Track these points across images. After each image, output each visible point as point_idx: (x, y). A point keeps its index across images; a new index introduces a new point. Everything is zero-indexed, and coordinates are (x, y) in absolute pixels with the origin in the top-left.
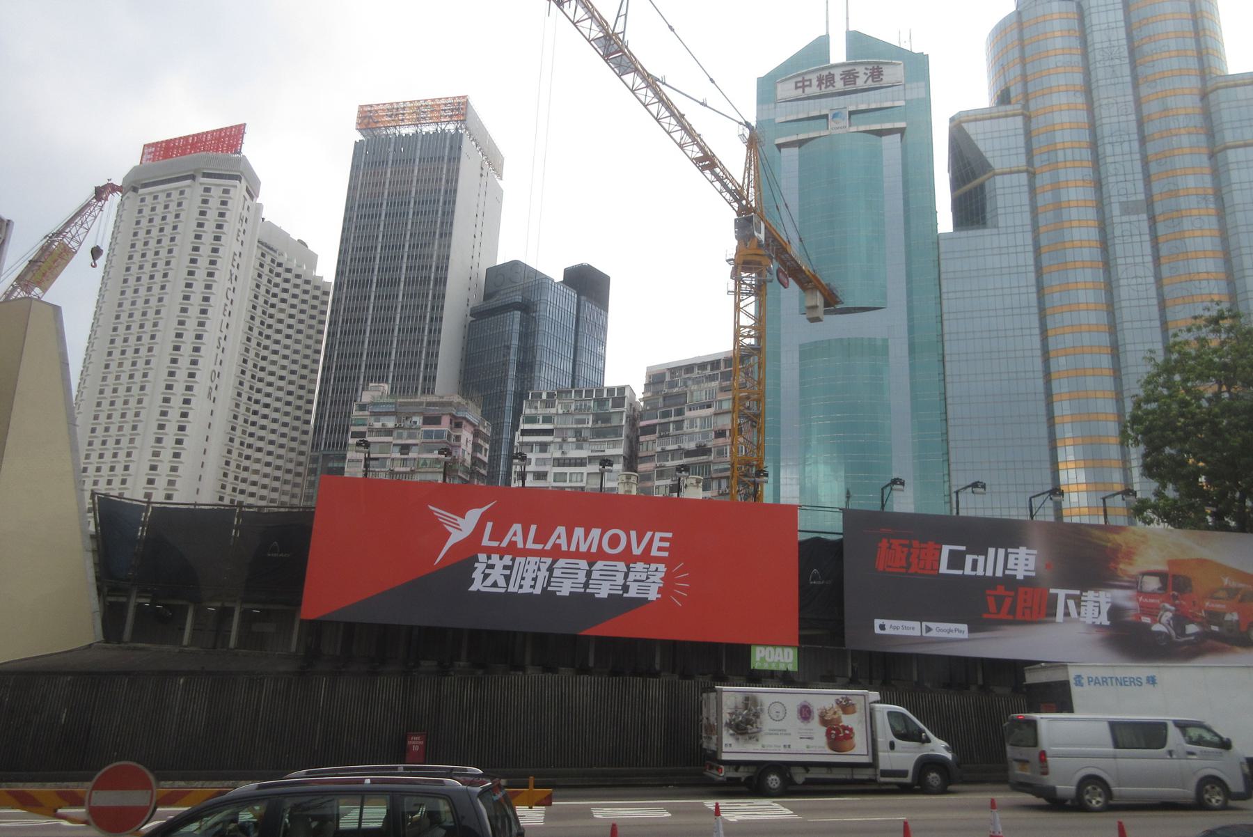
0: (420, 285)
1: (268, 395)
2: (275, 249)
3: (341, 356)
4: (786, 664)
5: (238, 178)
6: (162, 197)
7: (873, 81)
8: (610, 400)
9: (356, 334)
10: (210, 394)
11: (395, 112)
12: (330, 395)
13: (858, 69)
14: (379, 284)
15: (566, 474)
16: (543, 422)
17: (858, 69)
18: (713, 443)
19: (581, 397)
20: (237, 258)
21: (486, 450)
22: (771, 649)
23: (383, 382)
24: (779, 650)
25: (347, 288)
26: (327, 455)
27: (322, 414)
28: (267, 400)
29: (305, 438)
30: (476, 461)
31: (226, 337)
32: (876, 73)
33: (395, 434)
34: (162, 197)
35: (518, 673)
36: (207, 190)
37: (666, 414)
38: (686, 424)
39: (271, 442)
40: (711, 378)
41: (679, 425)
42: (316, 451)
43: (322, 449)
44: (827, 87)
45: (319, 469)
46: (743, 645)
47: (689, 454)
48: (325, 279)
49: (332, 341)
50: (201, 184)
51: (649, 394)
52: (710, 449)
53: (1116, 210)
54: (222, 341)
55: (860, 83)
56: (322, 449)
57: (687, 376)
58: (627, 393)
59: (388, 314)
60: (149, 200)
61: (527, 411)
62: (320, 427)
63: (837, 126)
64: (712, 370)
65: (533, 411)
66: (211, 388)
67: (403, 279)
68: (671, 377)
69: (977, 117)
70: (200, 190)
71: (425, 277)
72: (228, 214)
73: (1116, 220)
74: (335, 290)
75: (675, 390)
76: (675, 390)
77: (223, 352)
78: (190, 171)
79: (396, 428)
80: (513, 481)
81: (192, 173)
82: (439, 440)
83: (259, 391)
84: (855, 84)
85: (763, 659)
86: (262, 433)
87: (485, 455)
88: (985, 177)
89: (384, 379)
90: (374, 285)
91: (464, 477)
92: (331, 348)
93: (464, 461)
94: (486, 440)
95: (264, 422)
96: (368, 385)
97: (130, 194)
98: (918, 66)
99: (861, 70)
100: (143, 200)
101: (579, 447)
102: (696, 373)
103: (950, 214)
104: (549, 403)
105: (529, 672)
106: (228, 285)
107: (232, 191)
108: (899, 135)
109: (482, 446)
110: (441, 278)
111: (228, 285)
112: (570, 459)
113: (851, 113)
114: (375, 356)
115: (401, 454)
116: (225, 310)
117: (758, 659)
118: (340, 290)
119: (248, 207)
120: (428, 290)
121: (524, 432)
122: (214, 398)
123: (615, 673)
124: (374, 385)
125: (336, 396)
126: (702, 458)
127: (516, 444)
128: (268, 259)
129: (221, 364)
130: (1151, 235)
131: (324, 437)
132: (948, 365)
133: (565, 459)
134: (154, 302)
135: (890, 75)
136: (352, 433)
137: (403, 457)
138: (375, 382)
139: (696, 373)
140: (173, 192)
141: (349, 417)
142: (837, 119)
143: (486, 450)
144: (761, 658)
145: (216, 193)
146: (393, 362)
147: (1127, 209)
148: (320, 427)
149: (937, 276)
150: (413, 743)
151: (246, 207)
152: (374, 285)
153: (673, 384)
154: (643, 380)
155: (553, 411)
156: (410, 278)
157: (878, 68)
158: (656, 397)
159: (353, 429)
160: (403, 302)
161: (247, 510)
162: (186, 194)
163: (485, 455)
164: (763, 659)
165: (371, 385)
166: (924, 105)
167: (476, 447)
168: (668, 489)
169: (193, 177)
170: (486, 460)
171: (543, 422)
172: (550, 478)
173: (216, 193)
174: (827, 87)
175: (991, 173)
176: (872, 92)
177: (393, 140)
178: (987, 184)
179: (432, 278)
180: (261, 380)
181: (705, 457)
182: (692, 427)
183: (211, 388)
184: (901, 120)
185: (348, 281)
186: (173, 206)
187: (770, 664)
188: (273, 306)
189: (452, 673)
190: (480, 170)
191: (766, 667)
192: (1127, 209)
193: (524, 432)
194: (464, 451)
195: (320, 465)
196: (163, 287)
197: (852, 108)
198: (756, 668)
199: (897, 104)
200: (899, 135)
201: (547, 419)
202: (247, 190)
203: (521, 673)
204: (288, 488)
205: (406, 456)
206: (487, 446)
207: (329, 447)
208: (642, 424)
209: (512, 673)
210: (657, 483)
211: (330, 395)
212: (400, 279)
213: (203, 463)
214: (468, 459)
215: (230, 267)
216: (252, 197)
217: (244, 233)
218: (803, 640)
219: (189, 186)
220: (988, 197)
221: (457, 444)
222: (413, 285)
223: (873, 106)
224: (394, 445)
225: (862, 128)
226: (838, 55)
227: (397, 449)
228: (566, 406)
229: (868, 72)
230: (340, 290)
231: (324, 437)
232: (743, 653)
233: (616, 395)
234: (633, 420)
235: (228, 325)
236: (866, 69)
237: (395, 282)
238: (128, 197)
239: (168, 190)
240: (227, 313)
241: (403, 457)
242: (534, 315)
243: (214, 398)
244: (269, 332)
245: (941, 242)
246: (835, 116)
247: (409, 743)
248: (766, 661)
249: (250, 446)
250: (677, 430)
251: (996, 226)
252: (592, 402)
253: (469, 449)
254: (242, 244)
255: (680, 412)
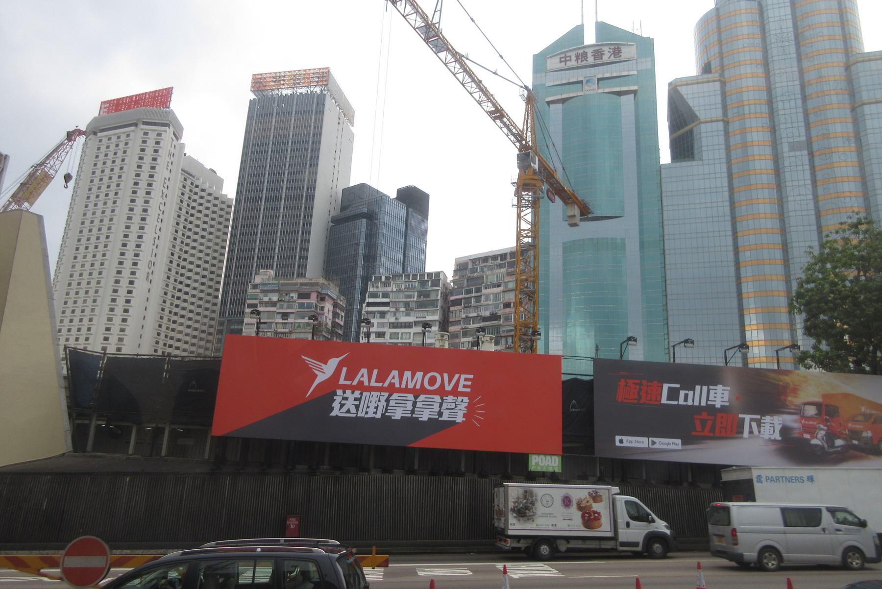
0: (296, 200)
1: (189, 278)
2: (194, 175)
3: (240, 250)
4: (553, 467)
5: (167, 125)
6: (114, 139)
7: (614, 57)
8: (430, 282)
9: (251, 235)
10: (148, 277)
11: (278, 79)
12: (232, 278)
13: (604, 48)
14: (267, 200)
15: (398, 333)
16: (382, 297)
17: (604, 48)
18: (502, 311)
19: (409, 279)
20: (167, 181)
21: (342, 316)
22: (543, 457)
23: (269, 269)
24: (548, 457)
25: (245, 203)
26: (230, 320)
27: (226, 291)
28: (188, 282)
29: (214, 308)
30: (335, 324)
31: (159, 237)
32: (617, 51)
33: (278, 305)
34: (114, 139)
35: (365, 473)
36: (146, 134)
37: (469, 292)
38: (483, 298)
39: (191, 311)
40: (500, 266)
41: (478, 299)
42: (222, 318)
43: (227, 316)
44: (582, 61)
45: (225, 330)
46: (523, 454)
47: (485, 319)
48: (229, 197)
49: (234, 240)
50: (142, 129)
51: (457, 277)
52: (500, 316)
53: (786, 148)
54: (156, 240)
55: (606, 58)
56: (227, 316)
57: (483, 265)
58: (441, 277)
59: (273, 221)
60: (105, 140)
61: (371, 289)
62: (225, 300)
63: (589, 89)
64: (501, 260)
65: (375, 289)
66: (148, 273)
67: (283, 196)
68: (473, 266)
69: (688, 82)
70: (141, 134)
71: (299, 195)
72: (160, 151)
73: (785, 155)
74: (236, 204)
75: (475, 274)
76: (475, 274)
77: (157, 247)
78: (134, 120)
79: (279, 301)
80: (361, 338)
81: (135, 122)
82: (309, 310)
83: (182, 275)
84: (602, 59)
85: (537, 464)
86: (185, 305)
87: (342, 320)
88: (694, 124)
89: (270, 267)
90: (263, 201)
91: (327, 335)
92: (233, 245)
93: (327, 324)
94: (342, 309)
95: (186, 297)
96: (259, 271)
97: (92, 136)
98: (646, 46)
99: (606, 49)
100: (100, 141)
101: (408, 315)
102: (490, 263)
103: (669, 151)
104: (386, 284)
105: (372, 473)
106: (161, 200)
107: (164, 134)
108: (633, 95)
109: (339, 314)
110: (310, 196)
111: (161, 200)
112: (401, 323)
113: (599, 80)
114: (264, 251)
115: (283, 320)
116: (158, 218)
117: (533, 464)
118: (239, 204)
119: (175, 146)
120: (301, 204)
121: (369, 304)
122: (151, 280)
123: (433, 473)
124: (263, 271)
125: (237, 279)
126: (494, 322)
127: (363, 312)
128: (189, 182)
129: (155, 256)
130: (810, 166)
131: (228, 307)
132: (667, 257)
133: (398, 323)
134: (108, 212)
135: (626, 53)
136: (248, 304)
137: (283, 321)
138: (264, 269)
139: (490, 263)
140: (122, 135)
141: (246, 293)
142: (589, 84)
143: (342, 316)
144: (536, 463)
145: (152, 136)
146: (277, 255)
147: (793, 147)
148: (225, 300)
149: (659, 194)
150: (291, 523)
151: (173, 146)
152: (263, 201)
153: (473, 270)
154: (453, 268)
155: (389, 289)
156: (288, 196)
157: (618, 48)
158: (462, 279)
159: (249, 302)
160: (283, 212)
161: (174, 359)
162: (131, 137)
163: (342, 320)
164: (537, 464)
165: (261, 271)
166: (651, 74)
167: (335, 315)
168: (470, 344)
169: (136, 125)
170: (342, 323)
171: (382, 297)
172: (387, 336)
173: (152, 136)
174: (582, 61)
175: (698, 122)
176: (614, 65)
177: (277, 99)
178: (695, 129)
179: (304, 196)
180: (183, 267)
181: (496, 322)
182: (487, 300)
183: (148, 273)
184: (634, 85)
185: (245, 198)
186: (122, 145)
187: (542, 467)
188: (192, 215)
189: (318, 474)
190: (338, 119)
191: (539, 469)
192: (793, 147)
193: (369, 304)
194: (326, 317)
195: (225, 327)
196: (115, 202)
197: (600, 76)
198: (532, 470)
199: (631, 73)
200: (633, 95)
201: (385, 295)
202: (174, 134)
203: (367, 474)
204: (202, 343)
205: (286, 321)
206: (343, 314)
207: (232, 314)
208: (452, 298)
209: (361, 473)
210: (463, 340)
211: (232, 278)
212: (281, 196)
213: (143, 326)
214: (330, 323)
215: (162, 188)
216: (177, 139)
217: (172, 164)
218: (565, 450)
219: (133, 131)
220: (695, 138)
221: (322, 312)
222: (290, 200)
223: (615, 75)
224: (277, 313)
225: (607, 90)
226: (590, 38)
227: (280, 316)
228: (398, 286)
229: (611, 51)
230: (239, 204)
231: (228, 307)
232: (523, 459)
233: (433, 278)
234: (445, 296)
235: (160, 228)
236: (610, 48)
237: (278, 199)
238: (90, 139)
239: (118, 134)
240: (160, 220)
241: (283, 321)
242: (376, 221)
243: (151, 280)
244: (189, 233)
245: (662, 170)
246: (587, 82)
247: (288, 523)
248: (539, 465)
249: (176, 314)
250: (476, 303)
251: (701, 159)
252: (417, 283)
253: (330, 316)
254: (170, 172)
255: (478, 290)
